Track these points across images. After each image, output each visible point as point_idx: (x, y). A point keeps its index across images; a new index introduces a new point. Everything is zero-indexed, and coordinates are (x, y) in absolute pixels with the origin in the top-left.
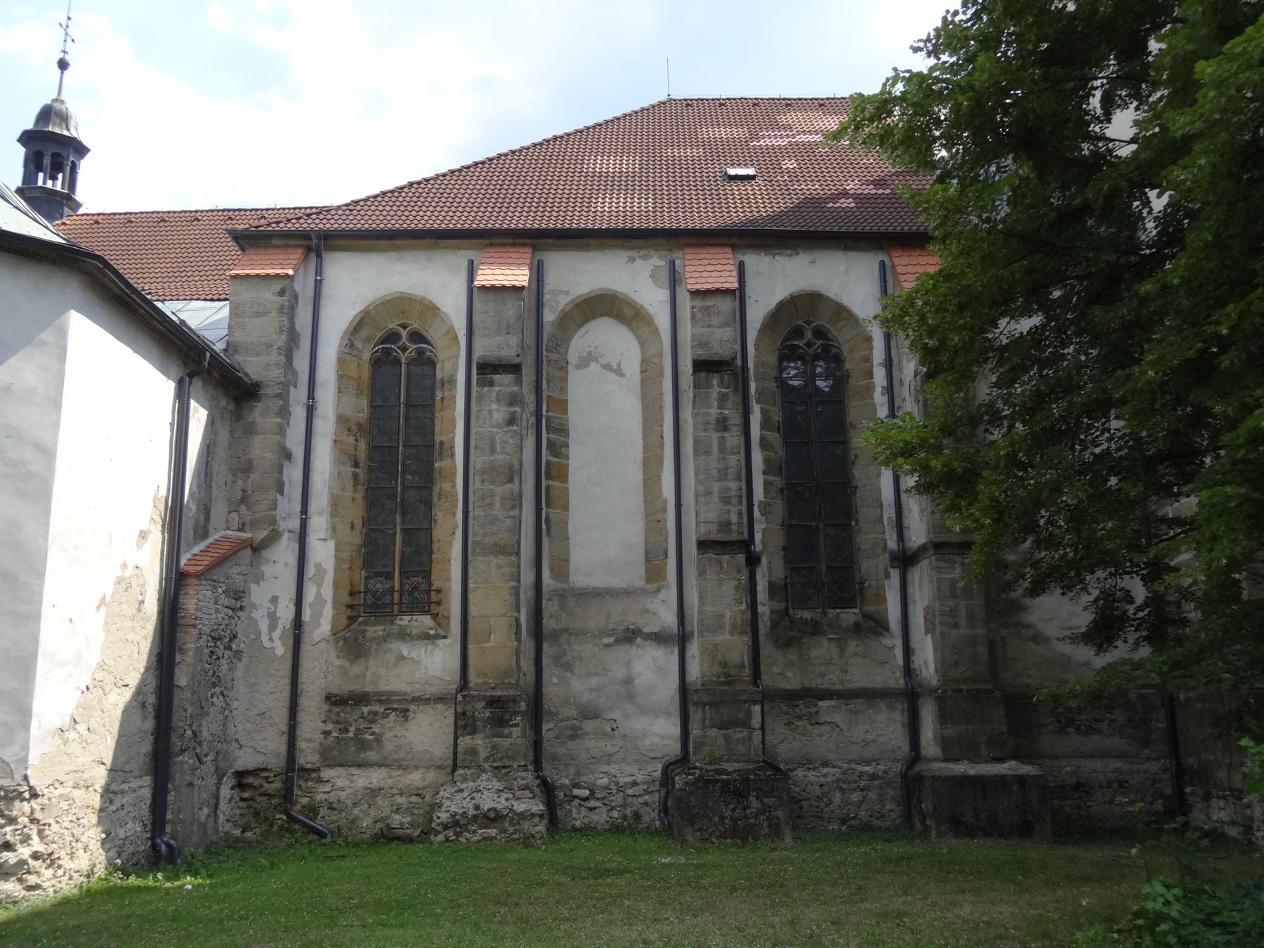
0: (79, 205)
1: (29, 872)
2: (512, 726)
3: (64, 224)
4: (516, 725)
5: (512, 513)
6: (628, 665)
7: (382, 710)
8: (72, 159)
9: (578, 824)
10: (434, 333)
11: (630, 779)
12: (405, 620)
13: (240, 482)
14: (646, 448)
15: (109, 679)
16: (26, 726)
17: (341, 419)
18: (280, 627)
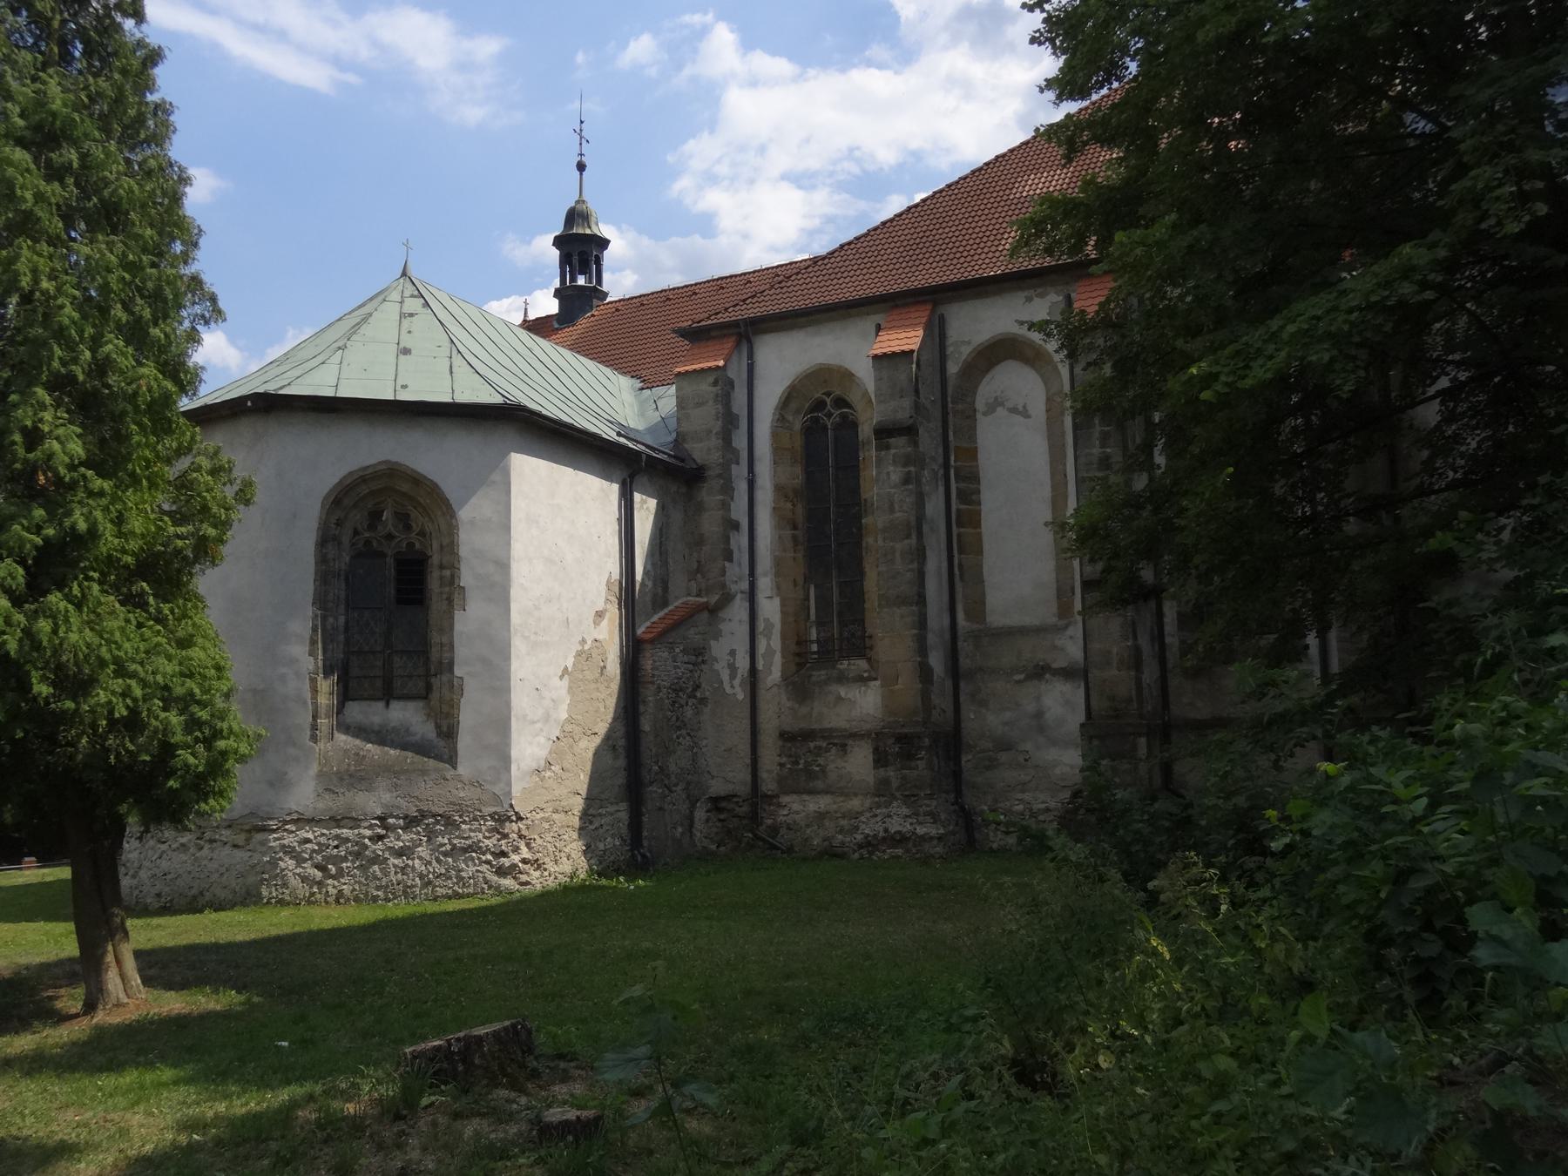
0: (605, 295)
1: (521, 873)
2: (919, 759)
3: (593, 316)
4: (922, 759)
5: (910, 567)
6: (1038, 698)
7: (824, 745)
8: (595, 253)
9: (995, 846)
10: (854, 398)
11: (1043, 806)
12: (844, 665)
13: (695, 554)
14: (1054, 488)
15: (578, 730)
16: (508, 769)
17: (779, 489)
18: (739, 676)
